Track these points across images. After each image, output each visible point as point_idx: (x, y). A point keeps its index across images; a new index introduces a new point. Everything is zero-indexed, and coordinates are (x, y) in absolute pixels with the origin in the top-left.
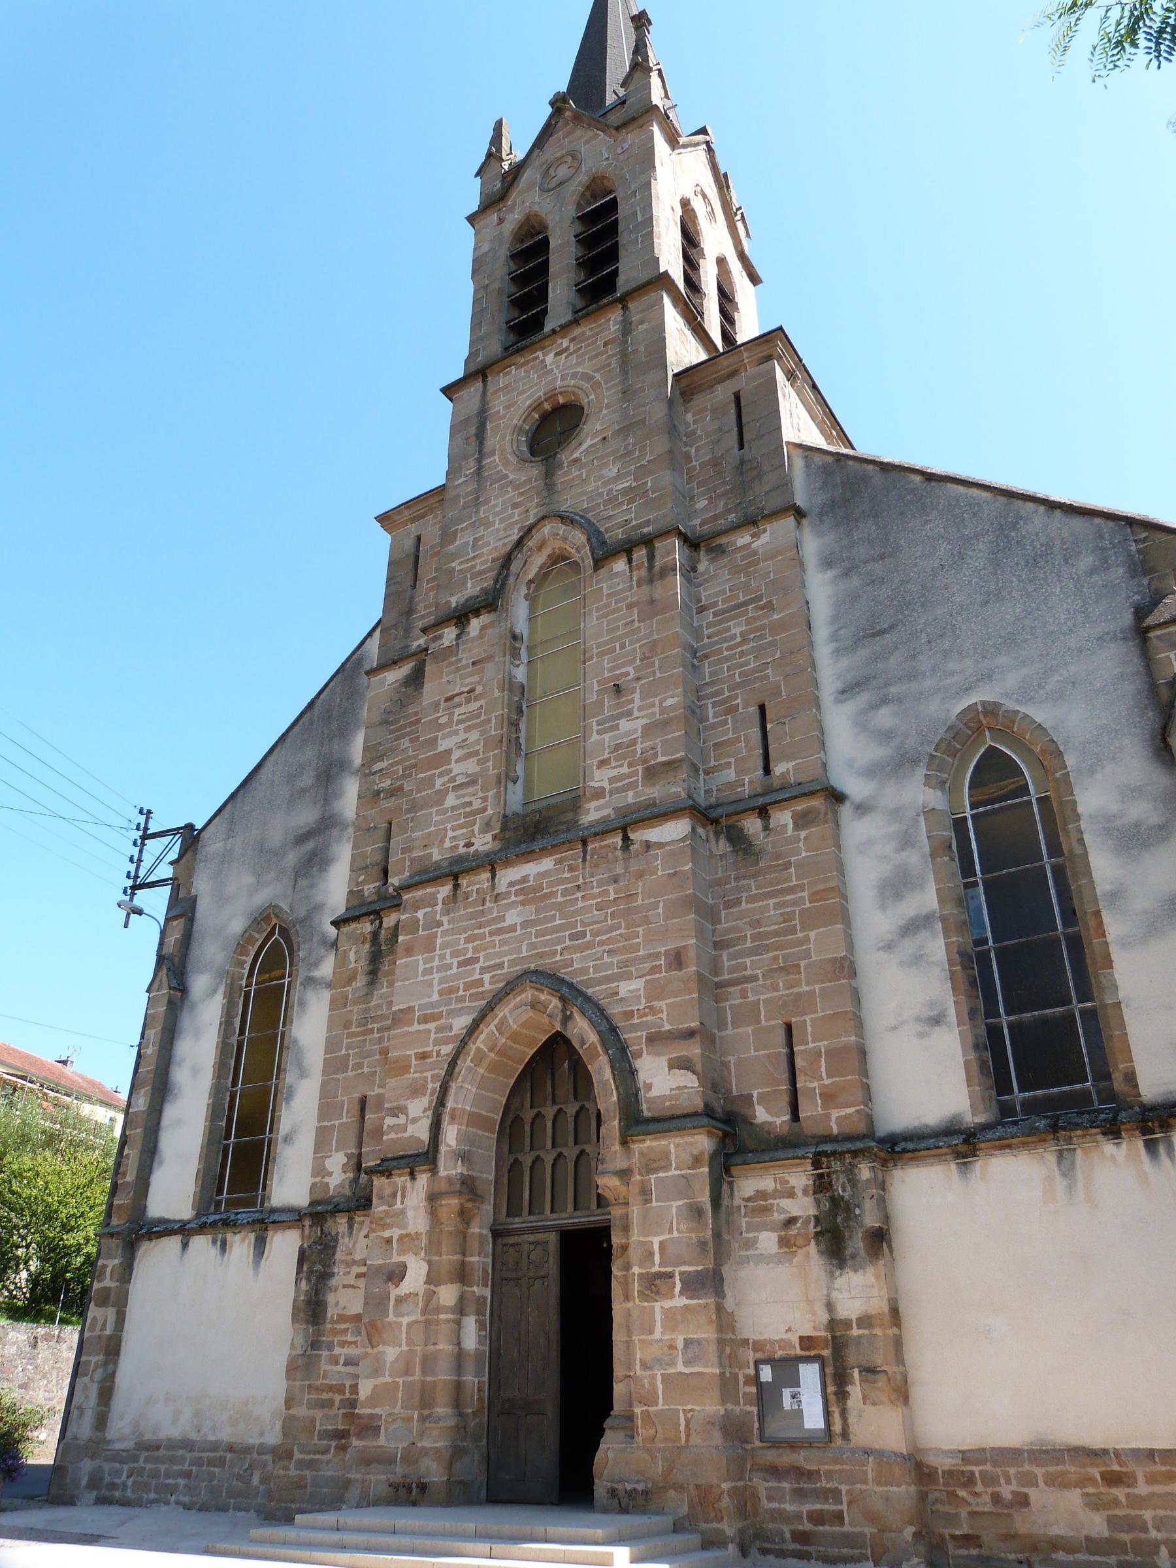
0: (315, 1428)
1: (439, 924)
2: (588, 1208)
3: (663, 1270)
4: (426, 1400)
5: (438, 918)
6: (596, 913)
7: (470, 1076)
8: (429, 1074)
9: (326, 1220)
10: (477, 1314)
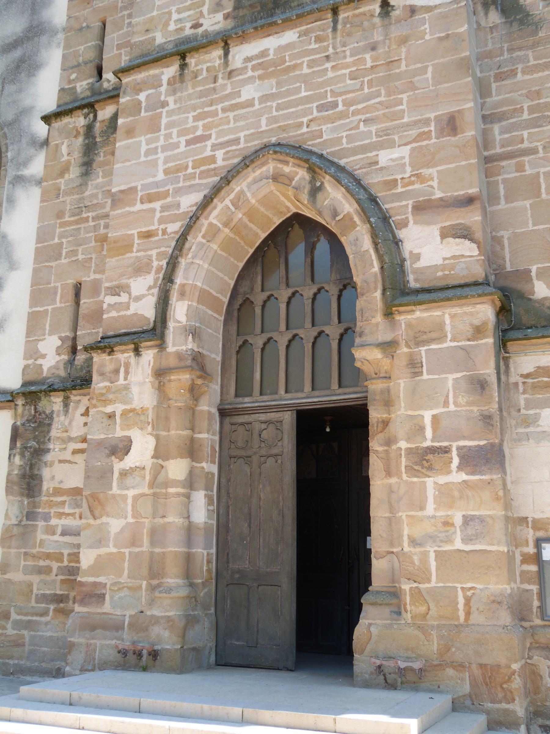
0: (32, 591)
1: (164, 104)
2: (329, 388)
3: (436, 444)
4: (155, 570)
5: (163, 98)
6: (349, 82)
7: (202, 253)
8: (154, 253)
9: (40, 399)
10: (206, 489)
